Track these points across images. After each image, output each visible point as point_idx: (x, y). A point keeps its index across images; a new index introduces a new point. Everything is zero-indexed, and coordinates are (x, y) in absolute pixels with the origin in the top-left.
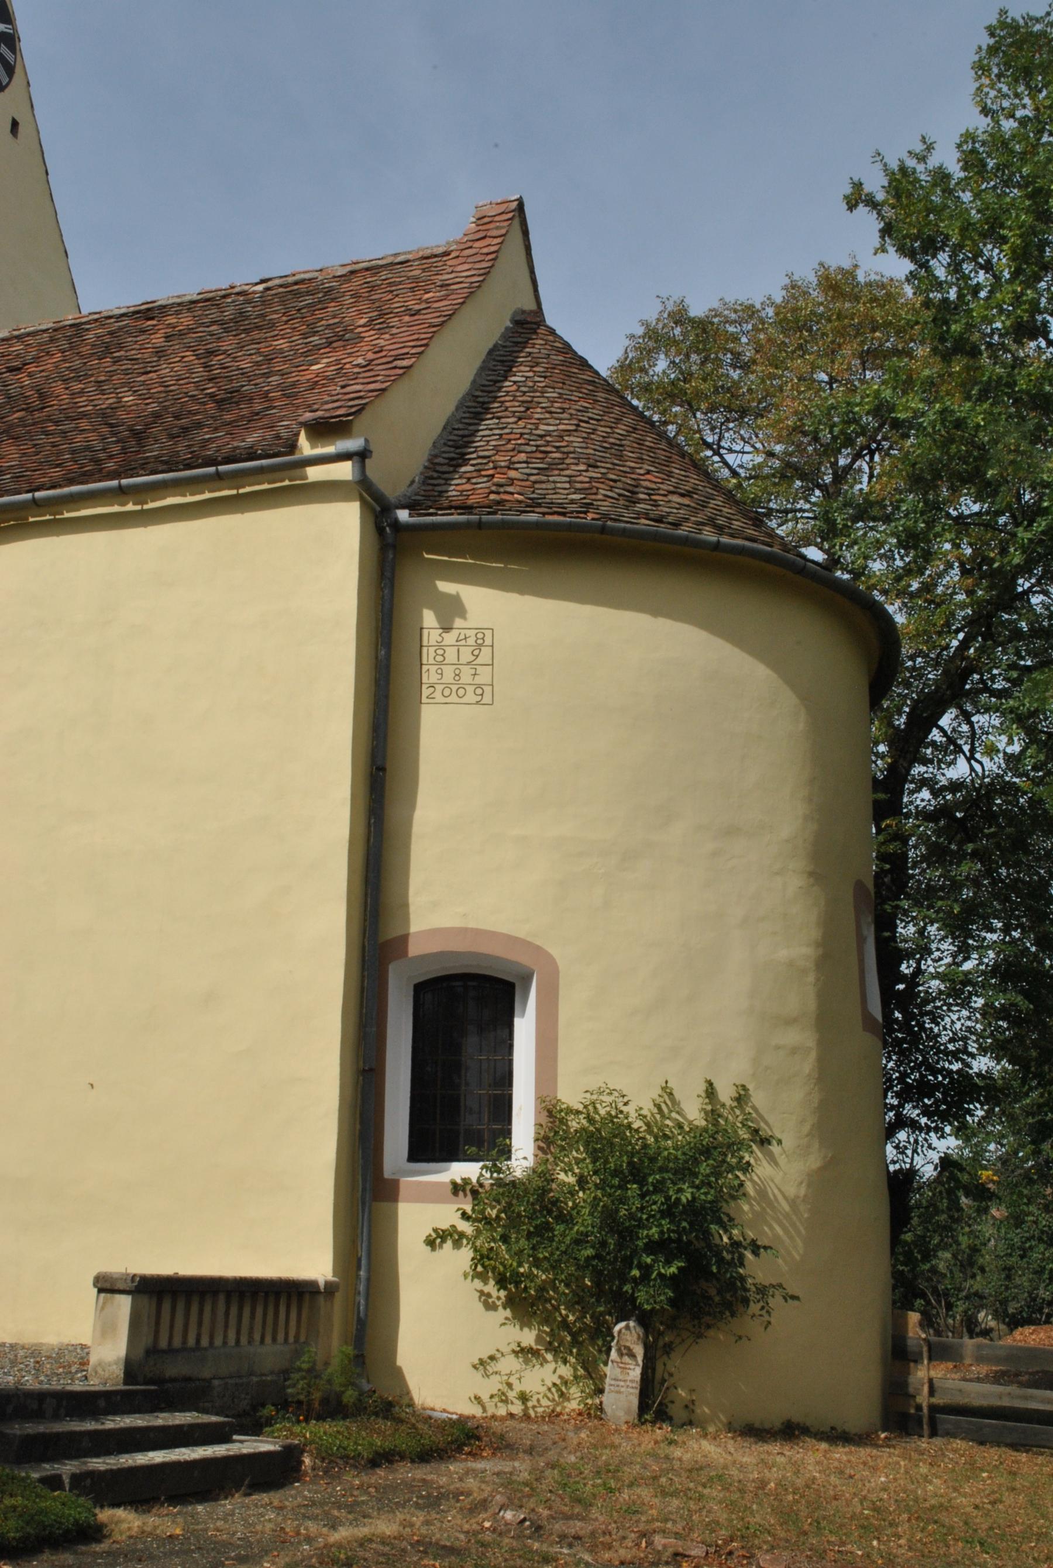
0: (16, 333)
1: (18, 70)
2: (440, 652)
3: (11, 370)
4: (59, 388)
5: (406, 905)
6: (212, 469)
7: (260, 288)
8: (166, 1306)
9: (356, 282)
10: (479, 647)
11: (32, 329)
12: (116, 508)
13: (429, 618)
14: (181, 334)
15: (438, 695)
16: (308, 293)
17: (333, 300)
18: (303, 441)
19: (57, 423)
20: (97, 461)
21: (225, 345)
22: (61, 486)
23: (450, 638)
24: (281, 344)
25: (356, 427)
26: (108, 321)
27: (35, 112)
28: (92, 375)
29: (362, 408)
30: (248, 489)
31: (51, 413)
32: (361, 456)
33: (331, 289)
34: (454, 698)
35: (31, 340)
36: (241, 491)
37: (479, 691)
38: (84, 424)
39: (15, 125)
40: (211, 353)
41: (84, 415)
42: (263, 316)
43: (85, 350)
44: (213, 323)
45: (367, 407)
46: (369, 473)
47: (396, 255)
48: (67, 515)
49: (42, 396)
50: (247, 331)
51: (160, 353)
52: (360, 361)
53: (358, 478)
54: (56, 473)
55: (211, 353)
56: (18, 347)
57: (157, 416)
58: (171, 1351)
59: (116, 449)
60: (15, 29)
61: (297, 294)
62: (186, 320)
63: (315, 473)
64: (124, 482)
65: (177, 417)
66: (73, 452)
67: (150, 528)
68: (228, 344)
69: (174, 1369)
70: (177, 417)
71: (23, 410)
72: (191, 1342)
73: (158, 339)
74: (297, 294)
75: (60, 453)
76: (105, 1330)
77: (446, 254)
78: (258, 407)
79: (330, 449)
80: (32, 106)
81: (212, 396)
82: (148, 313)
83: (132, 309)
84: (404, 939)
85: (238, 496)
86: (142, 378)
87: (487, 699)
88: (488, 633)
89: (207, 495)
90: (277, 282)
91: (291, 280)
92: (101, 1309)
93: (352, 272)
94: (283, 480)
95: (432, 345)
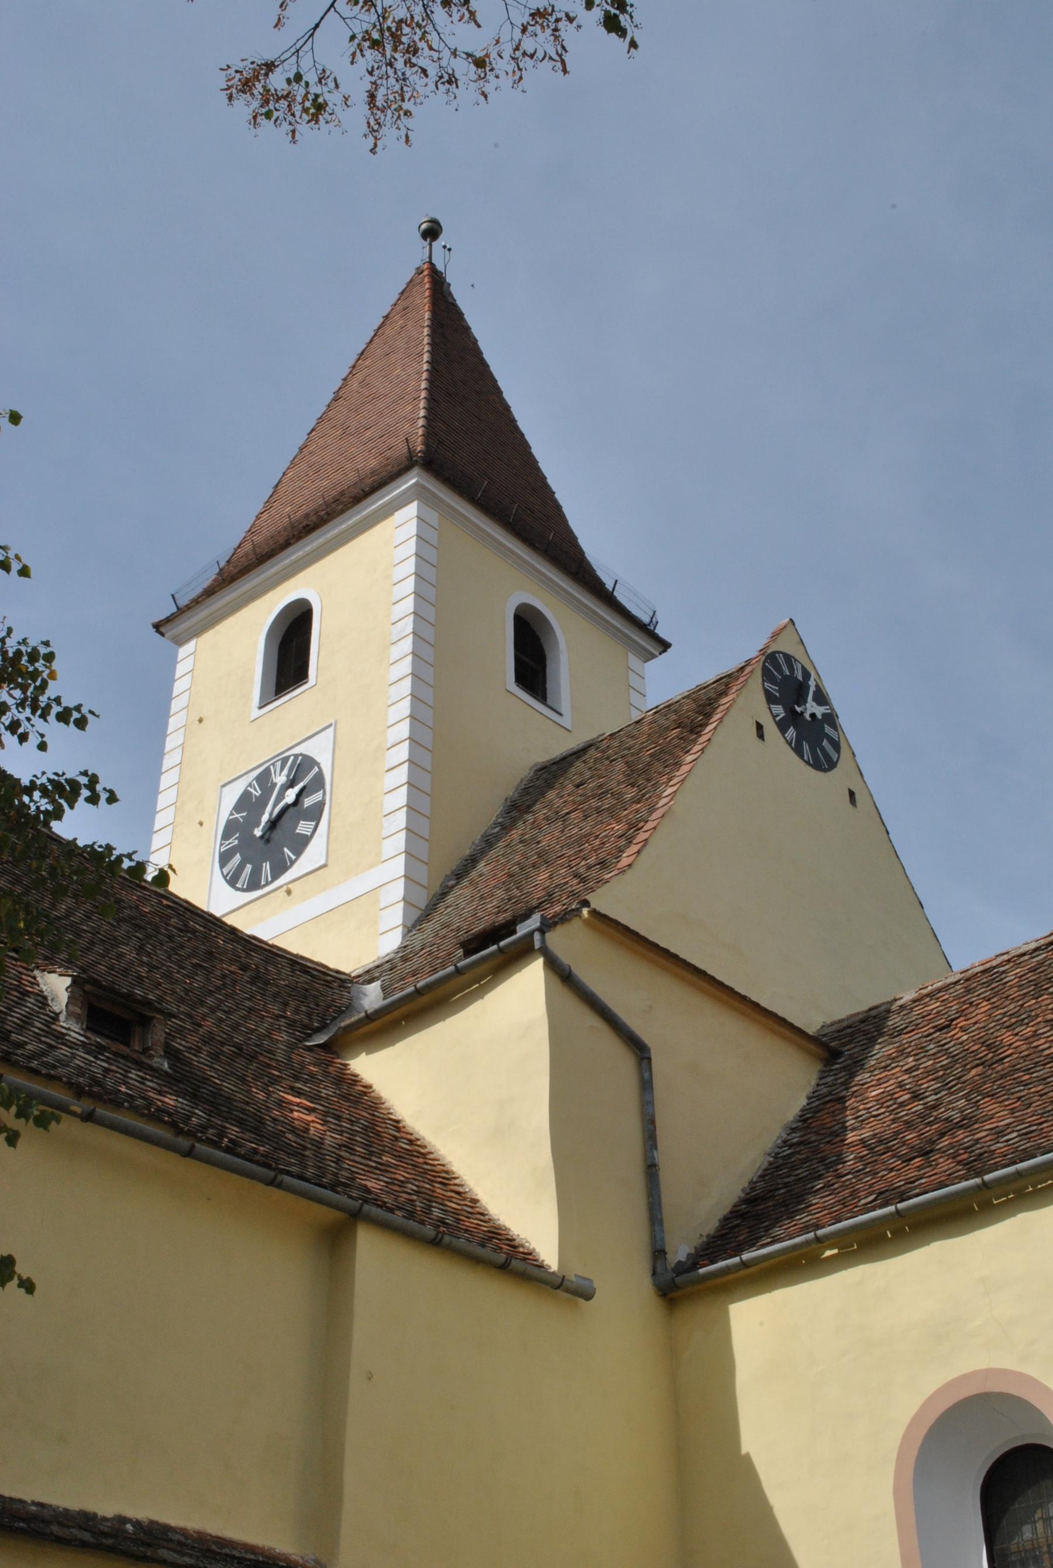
0: (924, 992)
1: (843, 744)
4: (1007, 1037)
11: (939, 984)
19: (1027, 1071)
26: (1022, 959)
27: (865, 779)
28: (1037, 1016)
31: (1013, 1063)
39: (852, 794)
60: (832, 709)
67: (849, 1270)
71: (977, 1065)
80: (861, 774)
83: (1042, 942)
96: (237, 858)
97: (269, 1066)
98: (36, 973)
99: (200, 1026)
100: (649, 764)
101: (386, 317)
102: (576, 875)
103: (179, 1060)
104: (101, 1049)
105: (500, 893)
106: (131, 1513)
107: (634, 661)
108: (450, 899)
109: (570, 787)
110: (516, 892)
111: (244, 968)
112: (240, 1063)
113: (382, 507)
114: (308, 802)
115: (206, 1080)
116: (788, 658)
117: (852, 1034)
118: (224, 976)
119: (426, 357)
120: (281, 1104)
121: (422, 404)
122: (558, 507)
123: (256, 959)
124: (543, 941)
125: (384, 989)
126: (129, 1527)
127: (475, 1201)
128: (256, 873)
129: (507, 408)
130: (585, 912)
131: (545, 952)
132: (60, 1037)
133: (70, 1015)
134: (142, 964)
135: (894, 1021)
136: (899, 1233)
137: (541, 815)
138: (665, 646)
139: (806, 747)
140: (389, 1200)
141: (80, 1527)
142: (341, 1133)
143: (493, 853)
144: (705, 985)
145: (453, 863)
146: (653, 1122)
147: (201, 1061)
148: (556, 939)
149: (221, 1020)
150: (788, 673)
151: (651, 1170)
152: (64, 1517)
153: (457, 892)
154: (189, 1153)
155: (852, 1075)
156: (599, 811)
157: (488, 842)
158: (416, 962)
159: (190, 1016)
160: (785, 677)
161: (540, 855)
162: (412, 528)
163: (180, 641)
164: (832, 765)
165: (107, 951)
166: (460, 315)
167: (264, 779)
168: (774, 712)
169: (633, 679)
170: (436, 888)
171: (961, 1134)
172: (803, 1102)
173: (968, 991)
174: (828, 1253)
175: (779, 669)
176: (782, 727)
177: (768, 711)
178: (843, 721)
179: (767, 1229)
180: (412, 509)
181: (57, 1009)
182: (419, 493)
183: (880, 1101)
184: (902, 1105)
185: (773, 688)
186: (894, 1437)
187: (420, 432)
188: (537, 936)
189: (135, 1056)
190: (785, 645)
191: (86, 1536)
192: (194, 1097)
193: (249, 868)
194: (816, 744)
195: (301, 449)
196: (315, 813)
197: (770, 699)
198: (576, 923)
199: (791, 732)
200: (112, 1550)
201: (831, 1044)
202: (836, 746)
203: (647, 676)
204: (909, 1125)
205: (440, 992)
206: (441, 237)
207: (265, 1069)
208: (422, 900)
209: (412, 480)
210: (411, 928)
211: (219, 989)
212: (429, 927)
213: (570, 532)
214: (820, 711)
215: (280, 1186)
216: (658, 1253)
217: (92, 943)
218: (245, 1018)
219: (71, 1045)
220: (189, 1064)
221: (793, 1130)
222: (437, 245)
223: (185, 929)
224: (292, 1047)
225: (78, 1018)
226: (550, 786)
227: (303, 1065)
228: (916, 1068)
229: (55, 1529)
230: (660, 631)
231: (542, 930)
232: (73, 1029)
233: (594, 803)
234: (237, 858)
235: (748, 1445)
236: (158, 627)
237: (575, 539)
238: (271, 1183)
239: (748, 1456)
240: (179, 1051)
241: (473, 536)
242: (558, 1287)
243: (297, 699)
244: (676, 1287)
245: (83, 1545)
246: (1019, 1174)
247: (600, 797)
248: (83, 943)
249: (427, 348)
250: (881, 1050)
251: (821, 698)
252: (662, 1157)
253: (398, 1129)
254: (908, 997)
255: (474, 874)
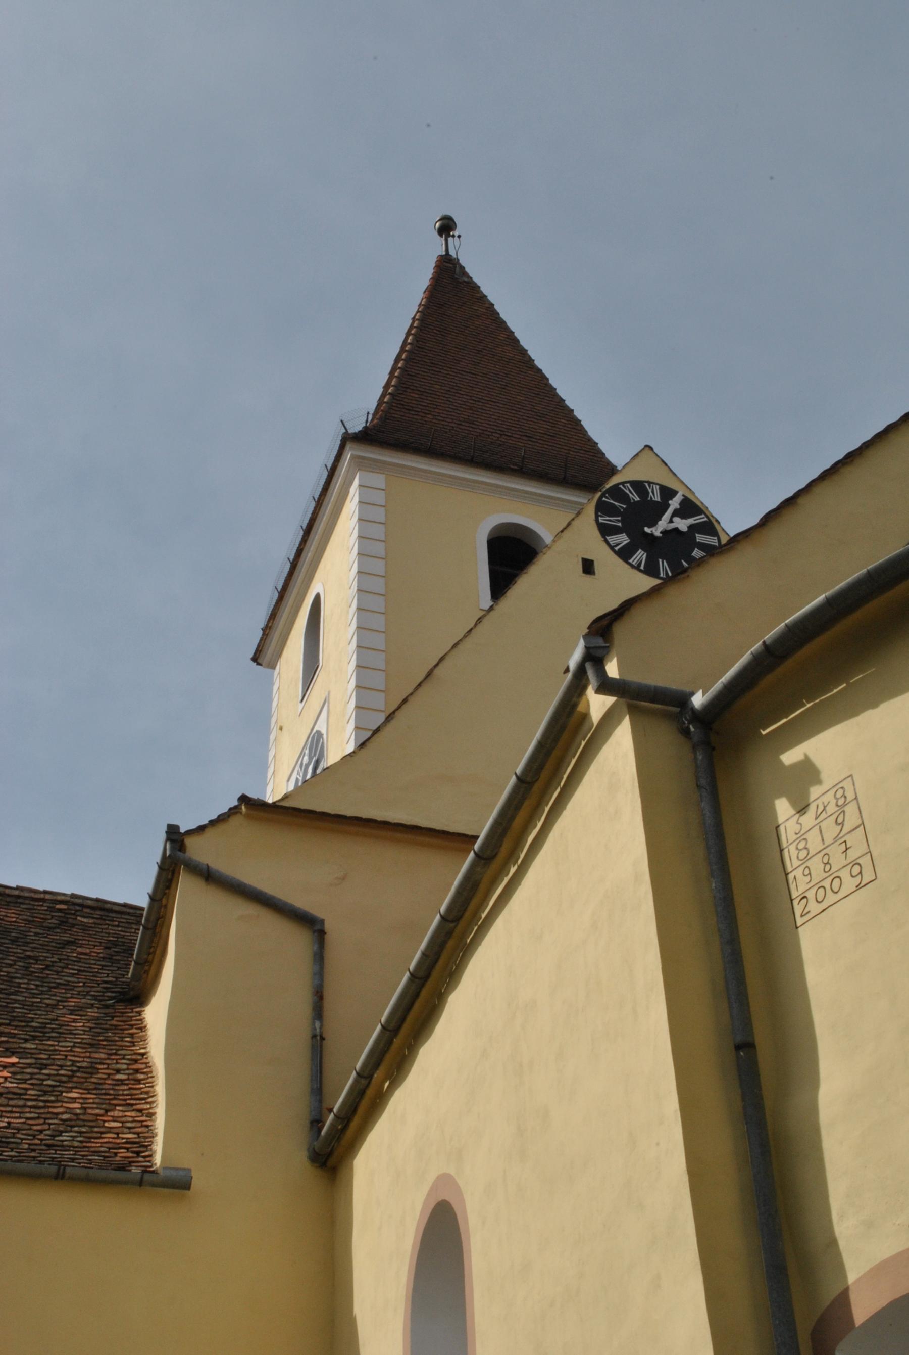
2: (801, 846)
5: (833, 1242)
10: (841, 809)
13: (783, 808)
15: (814, 907)
23: (808, 819)
34: (831, 898)
36: (562, 784)
37: (856, 870)
48: (483, 916)
84: (843, 1299)
87: (868, 876)
88: (847, 784)
94: (580, 744)
150: (637, 499)
168: (611, 543)
177: (604, 544)
182: (360, 464)
197: (605, 531)
199: (640, 556)
201: (168, 855)
207: (134, 1086)
241: (431, 482)
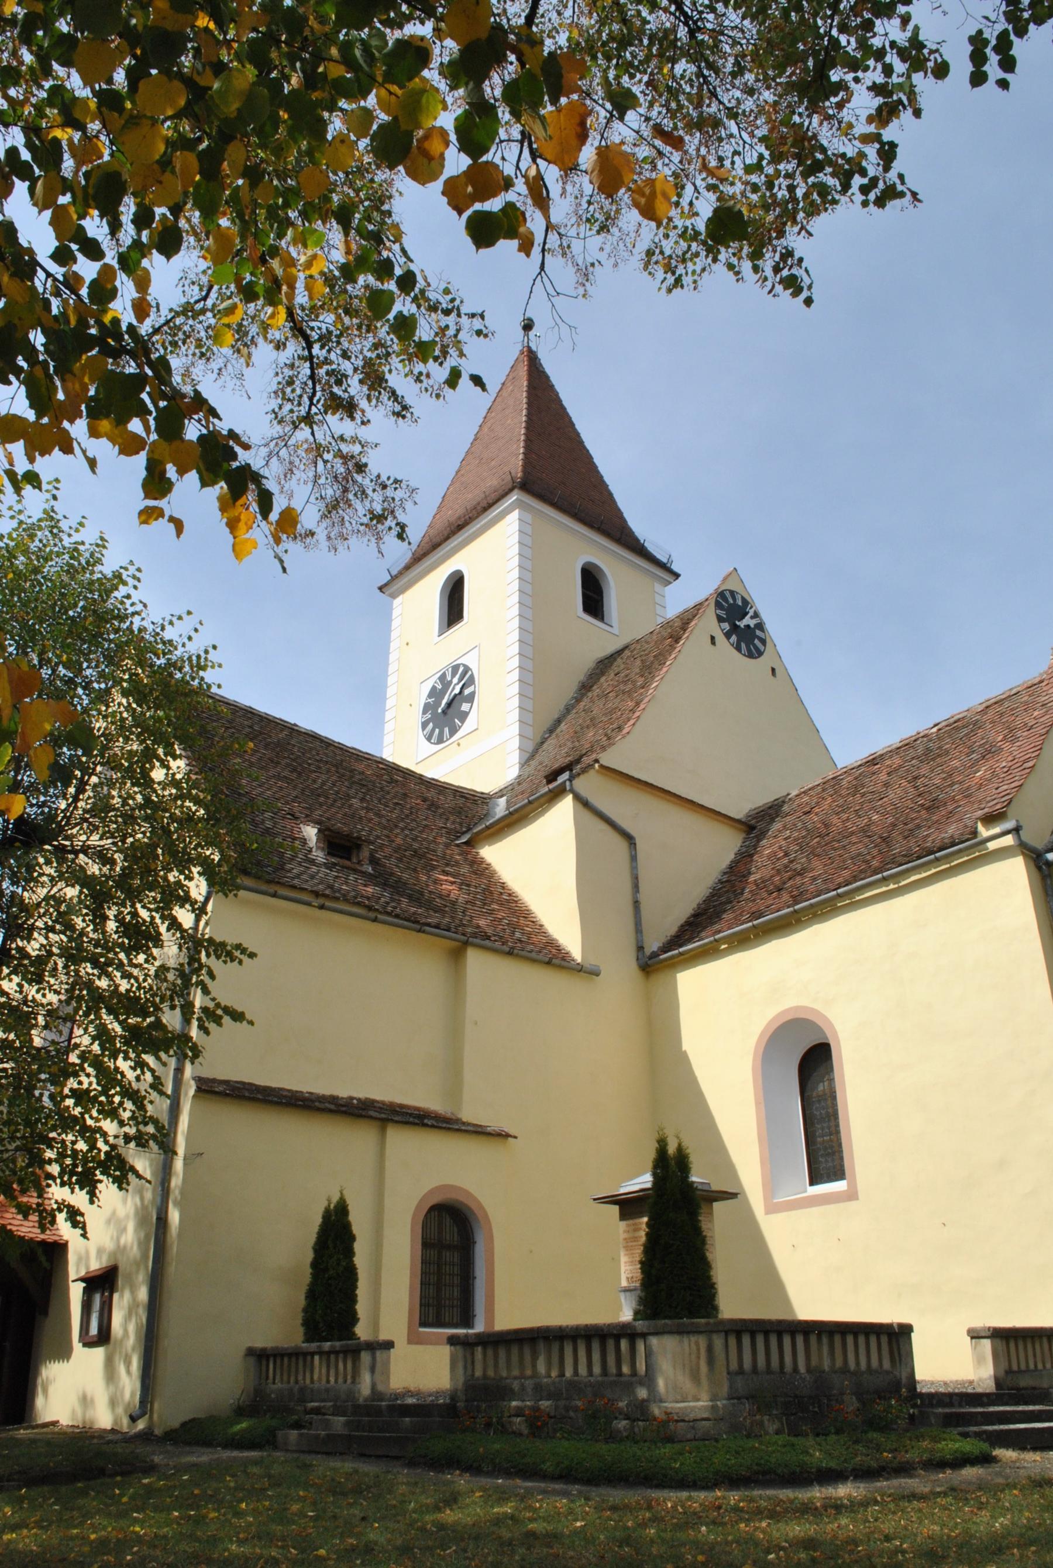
1: (768, 640)
3: (805, 813)
6: (932, 857)
7: (935, 730)
8: (1012, 1345)
9: (991, 713)
12: (884, 889)
14: (896, 770)
16: (964, 727)
17: (979, 728)
18: (980, 828)
19: (839, 841)
20: (867, 862)
21: (923, 772)
22: (851, 883)
24: (955, 763)
25: (1009, 814)
29: (1010, 801)
30: (956, 862)
32: (1017, 830)
33: (977, 721)
35: (812, 793)
38: (854, 839)
39: (773, 670)
40: (916, 778)
41: (852, 833)
42: (939, 748)
43: (844, 792)
44: (913, 758)
45: (1014, 800)
46: (1023, 838)
47: (1011, 690)
48: (858, 898)
49: (826, 826)
50: (933, 759)
51: (886, 785)
52: (1004, 764)
53: (1018, 843)
54: (846, 873)
55: (916, 778)
56: (806, 799)
57: (894, 825)
58: (1020, 1371)
59: (875, 852)
60: (761, 619)
61: (957, 729)
62: (897, 761)
63: (992, 845)
64: (885, 874)
65: (905, 824)
66: (852, 858)
68: (924, 770)
69: (1024, 1382)
70: (905, 824)
72: (1032, 1366)
73: (883, 777)
74: (957, 729)
75: (844, 861)
76: (979, 1360)
77: (1041, 682)
78: (950, 808)
79: (997, 830)
81: (922, 805)
82: (873, 761)
85: (951, 868)
86: (880, 803)
89: (933, 871)
90: (944, 724)
91: (952, 720)
92: (974, 1348)
93: (987, 707)
95: (1045, 746)
96: (431, 725)
97: (432, 860)
98: (301, 826)
99: (393, 841)
100: (652, 663)
101: (503, 384)
102: (606, 735)
103: (378, 864)
104: (335, 864)
105: (569, 744)
106: (355, 1095)
107: (658, 587)
108: (545, 746)
109: (612, 675)
110: (577, 744)
111: (425, 800)
112: (415, 862)
113: (496, 516)
114: (467, 692)
115: (392, 874)
116: (733, 593)
117: (763, 816)
118: (412, 808)
119: (524, 412)
120: (436, 882)
121: (522, 444)
122: (610, 495)
123: (431, 794)
124: (571, 785)
125: (508, 801)
126: (355, 1102)
127: (541, 926)
128: (441, 734)
129: (578, 435)
130: (597, 765)
131: (572, 791)
132: (313, 862)
133: (318, 848)
134: (363, 808)
135: (786, 808)
136: (756, 936)
137: (595, 694)
138: (677, 576)
139: (743, 645)
140: (490, 931)
141: (329, 1103)
142: (469, 894)
143: (569, 717)
144: (672, 799)
145: (548, 723)
146: (637, 878)
147: (391, 864)
148: (580, 784)
149: (407, 836)
151: (636, 904)
152: (322, 1099)
153: (549, 742)
154: (375, 920)
155: (759, 841)
156: (624, 693)
157: (568, 710)
158: (525, 785)
159: (388, 837)
160: (730, 605)
161: (592, 720)
162: (516, 526)
163: (394, 596)
164: (760, 653)
165: (343, 804)
166: (547, 377)
167: (442, 678)
169: (658, 599)
170: (538, 740)
171: (798, 878)
172: (732, 856)
173: (824, 790)
174: (723, 947)
175: (726, 601)
176: (728, 635)
178: (769, 626)
179: (700, 932)
180: (515, 515)
181: (311, 845)
182: (519, 504)
183: (769, 858)
184: (778, 859)
185: (722, 613)
186: (752, 1041)
187: (520, 463)
188: (568, 783)
189: (352, 866)
190: (730, 586)
191: (332, 1107)
192: (385, 885)
193: (437, 730)
194: (749, 642)
195: (457, 473)
196: (471, 698)
197: (720, 619)
198: (592, 773)
200: (345, 1113)
202: (763, 642)
203: (667, 595)
204: (779, 872)
205: (523, 812)
206: (534, 329)
208: (530, 747)
209: (514, 497)
210: (524, 764)
211: (407, 816)
212: (533, 763)
213: (619, 510)
214: (752, 623)
215: (424, 932)
216: (640, 948)
217: (335, 801)
218: (421, 832)
219: (319, 865)
220: (384, 866)
221: (725, 873)
222: (532, 334)
223: (392, 781)
224: (447, 846)
225: (323, 849)
226: (603, 673)
227: (451, 856)
228: (789, 837)
229: (317, 1104)
230: (675, 567)
231: (570, 780)
232: (319, 856)
233: (622, 687)
234: (431, 725)
235: (686, 1046)
236: (381, 589)
237: (621, 513)
238: (419, 931)
239: (685, 1052)
240: (379, 859)
242: (580, 971)
243: (458, 629)
244: (649, 966)
245: (331, 1111)
246: (812, 905)
247: (625, 682)
248: (330, 801)
249: (525, 406)
250: (777, 826)
251: (756, 615)
252: (642, 897)
253: (503, 888)
254: (794, 793)
255: (559, 730)
